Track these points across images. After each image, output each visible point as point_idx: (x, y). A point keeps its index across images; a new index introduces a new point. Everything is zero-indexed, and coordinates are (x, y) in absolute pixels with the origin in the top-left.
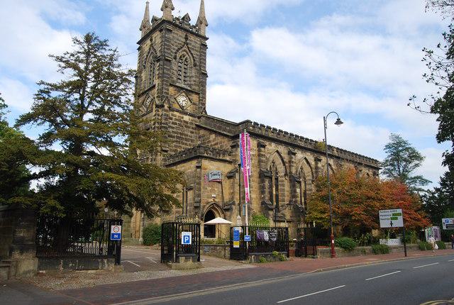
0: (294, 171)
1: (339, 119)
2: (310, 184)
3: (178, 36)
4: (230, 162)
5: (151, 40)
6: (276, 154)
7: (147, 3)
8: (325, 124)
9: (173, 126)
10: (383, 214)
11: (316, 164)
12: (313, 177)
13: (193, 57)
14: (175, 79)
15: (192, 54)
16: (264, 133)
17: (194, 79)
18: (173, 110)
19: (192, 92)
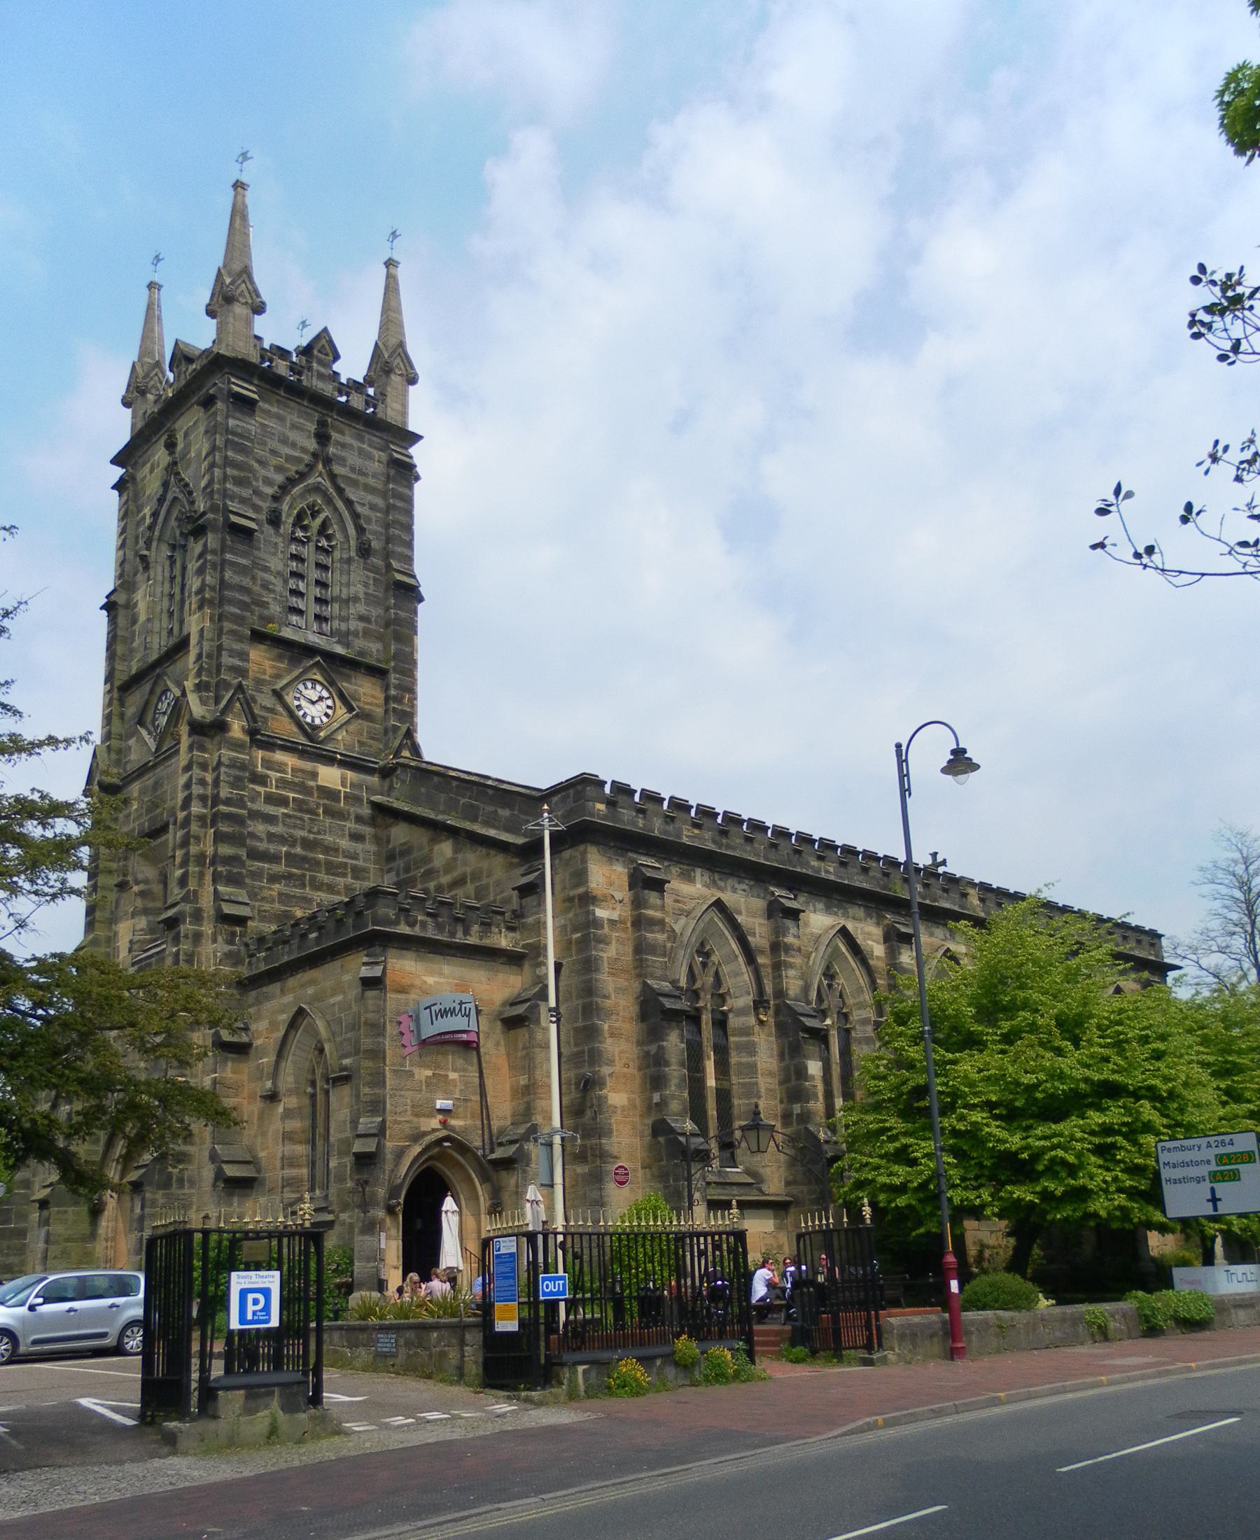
5: (170, 446)
13: (356, 516)
15: (349, 503)
16: (657, 828)
17: (361, 608)
18: (269, 745)
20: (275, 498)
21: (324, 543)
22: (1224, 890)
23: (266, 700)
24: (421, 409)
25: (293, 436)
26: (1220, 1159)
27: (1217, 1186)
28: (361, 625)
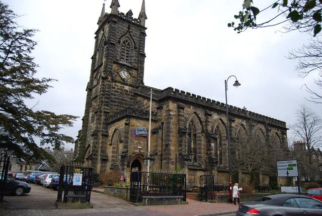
0: (209, 128)
1: (237, 82)
2: (225, 140)
3: (124, 27)
7: (104, 4)
8: (226, 86)
9: (115, 93)
13: (134, 42)
14: (118, 58)
15: (133, 40)
16: (184, 98)
17: (134, 58)
18: (116, 82)
19: (132, 68)
24: (147, 24)
27: (289, 171)
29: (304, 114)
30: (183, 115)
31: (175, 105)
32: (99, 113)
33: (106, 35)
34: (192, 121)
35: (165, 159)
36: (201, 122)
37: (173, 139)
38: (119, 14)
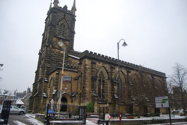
4: (77, 72)
6: (103, 68)
8: (118, 47)
10: (157, 99)
11: (128, 74)
12: (126, 80)
13: (68, 24)
14: (57, 34)
15: (67, 23)
16: (96, 57)
17: (68, 34)
18: (55, 48)
19: (66, 40)
20: (58, 22)
21: (64, 27)
22: (175, 70)
23: (55, 43)
24: (77, 13)
25: (61, 16)
26: (163, 100)
27: (163, 104)
28: (67, 36)
29: (178, 69)
30: (95, 68)
31: (90, 61)
32: (43, 68)
33: (50, 21)
34: (102, 72)
35: (82, 97)
36: (108, 73)
37: (88, 83)
38: (59, 8)
